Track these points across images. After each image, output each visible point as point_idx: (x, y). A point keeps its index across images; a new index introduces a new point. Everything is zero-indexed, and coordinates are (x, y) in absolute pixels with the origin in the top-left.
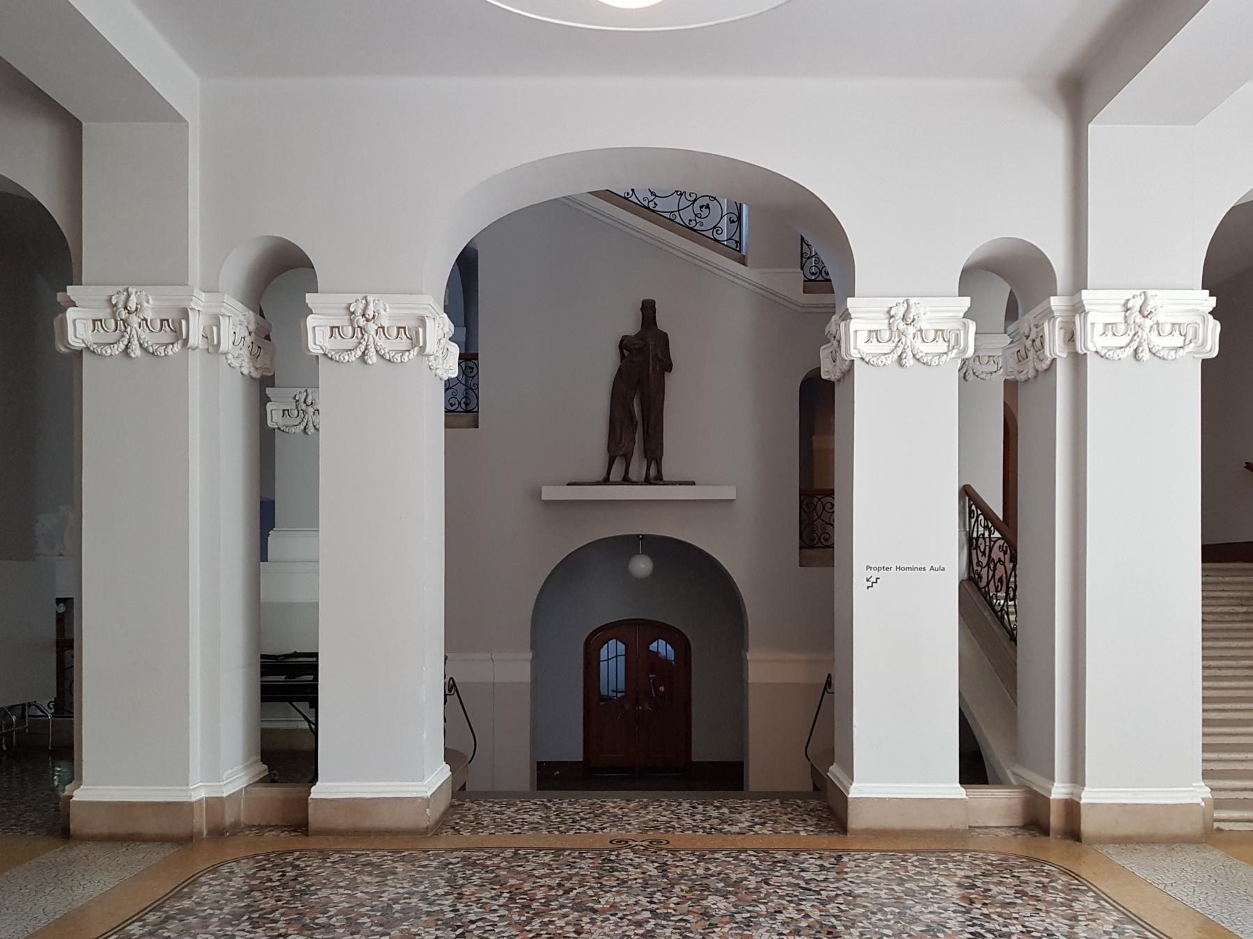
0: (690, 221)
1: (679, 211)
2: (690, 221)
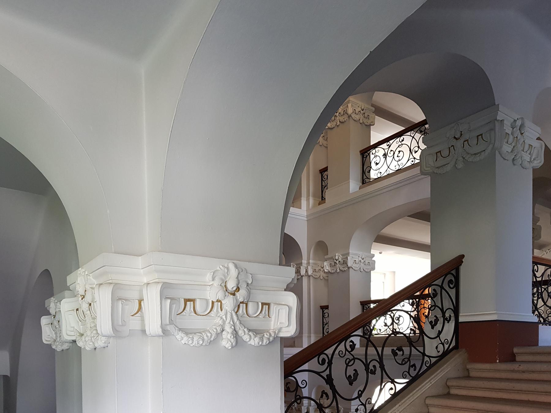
1: (388, 167)
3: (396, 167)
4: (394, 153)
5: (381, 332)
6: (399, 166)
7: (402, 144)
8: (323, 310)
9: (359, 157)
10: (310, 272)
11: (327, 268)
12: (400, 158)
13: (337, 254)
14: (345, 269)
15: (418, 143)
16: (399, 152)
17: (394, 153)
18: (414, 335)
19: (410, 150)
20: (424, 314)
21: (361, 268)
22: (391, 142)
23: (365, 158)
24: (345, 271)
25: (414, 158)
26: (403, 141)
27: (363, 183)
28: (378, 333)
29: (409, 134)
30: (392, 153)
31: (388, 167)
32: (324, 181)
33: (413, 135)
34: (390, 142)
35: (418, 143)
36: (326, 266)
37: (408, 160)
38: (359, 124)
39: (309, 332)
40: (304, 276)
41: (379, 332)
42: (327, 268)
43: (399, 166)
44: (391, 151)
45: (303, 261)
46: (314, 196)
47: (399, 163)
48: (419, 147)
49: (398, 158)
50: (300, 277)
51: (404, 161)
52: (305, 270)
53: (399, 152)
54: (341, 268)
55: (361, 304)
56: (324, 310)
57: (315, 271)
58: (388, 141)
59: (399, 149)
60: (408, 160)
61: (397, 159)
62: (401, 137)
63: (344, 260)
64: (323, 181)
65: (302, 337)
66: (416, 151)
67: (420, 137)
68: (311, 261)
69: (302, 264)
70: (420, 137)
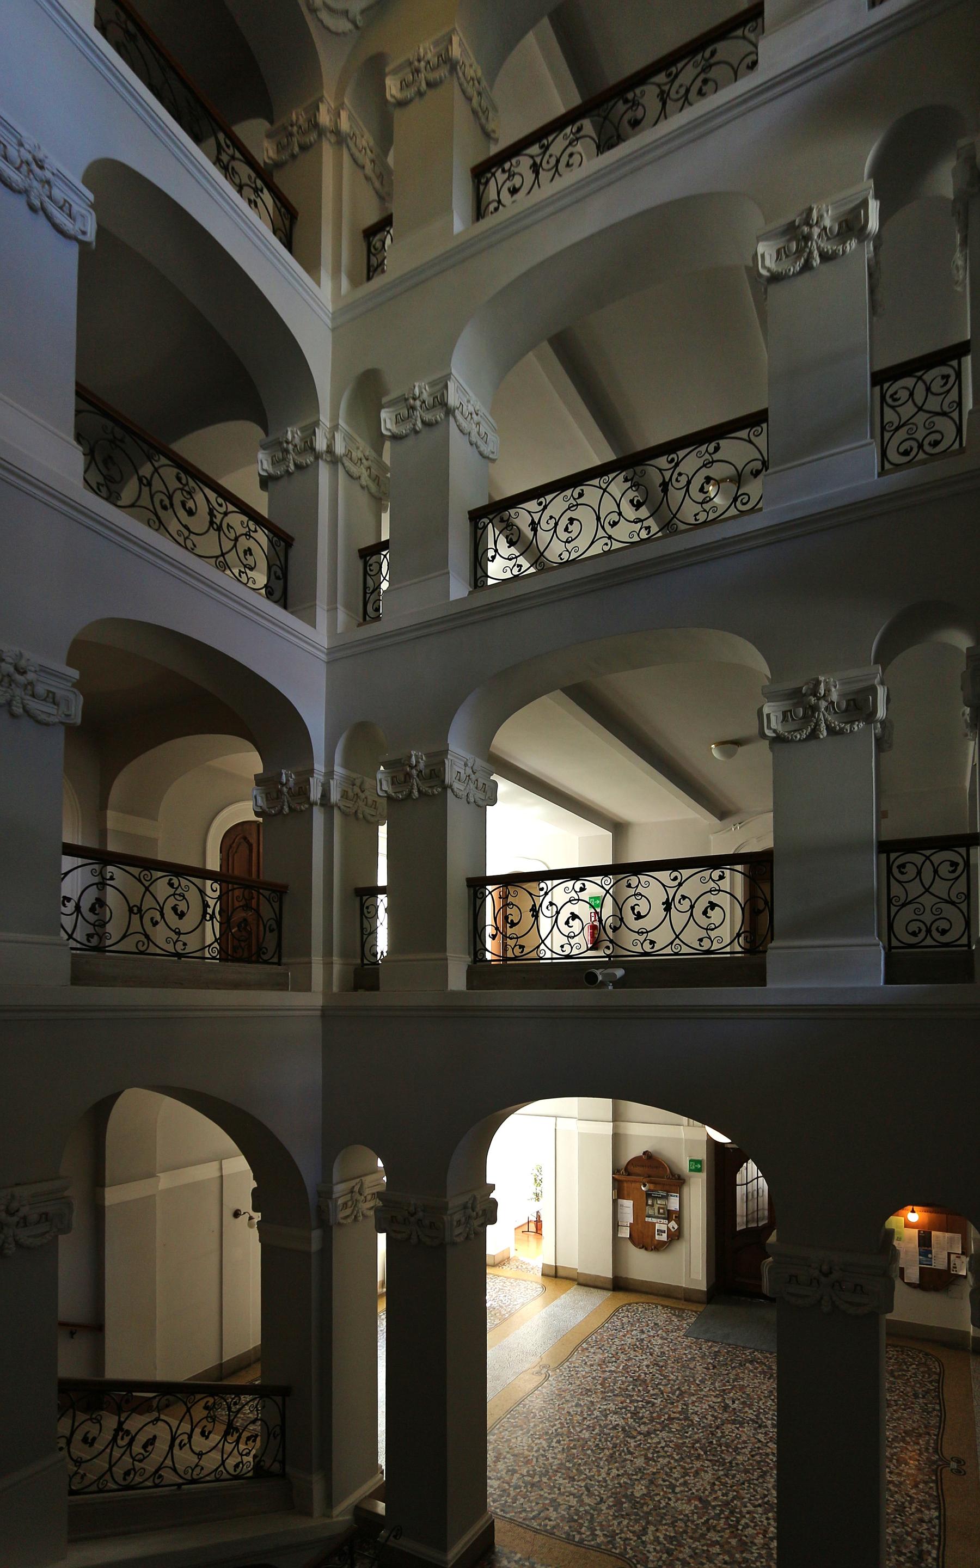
0: (701, 940)
2: (701, 940)
3: (698, 517)
4: (556, 524)
5: (526, 951)
6: (570, 553)
7: (577, 505)
8: (361, 900)
9: (466, 525)
10: (335, 796)
11: (385, 787)
12: (573, 535)
13: (413, 753)
14: (302, 807)
15: (618, 506)
16: (706, 478)
17: (556, 524)
18: (607, 959)
19: (598, 519)
20: (633, 908)
21: (471, 795)
22: (681, 453)
23: (481, 529)
24: (302, 811)
25: (610, 537)
26: (581, 495)
27: (365, 619)
28: (516, 957)
29: (596, 482)
30: (552, 522)
31: (677, 937)
32: (370, 575)
33: (604, 486)
34: (678, 453)
35: (618, 506)
36: (380, 781)
37: (593, 543)
38: (359, 488)
39: (328, 952)
40: (316, 804)
41: (518, 954)
42: (385, 787)
43: (570, 553)
44: (551, 517)
45: (316, 766)
46: (348, 606)
47: (569, 546)
48: (620, 514)
49: (567, 535)
50: (307, 806)
51: (582, 543)
52: (320, 789)
53: (571, 520)
54: (424, 788)
55: (468, 886)
56: (365, 898)
57: (345, 795)
58: (674, 451)
59: (569, 514)
60: (593, 543)
61: (564, 536)
62: (575, 488)
63: (432, 768)
64: (368, 577)
65: (311, 963)
66: (614, 521)
67: (904, 404)
68: (338, 769)
69: (313, 772)
70: (904, 404)
